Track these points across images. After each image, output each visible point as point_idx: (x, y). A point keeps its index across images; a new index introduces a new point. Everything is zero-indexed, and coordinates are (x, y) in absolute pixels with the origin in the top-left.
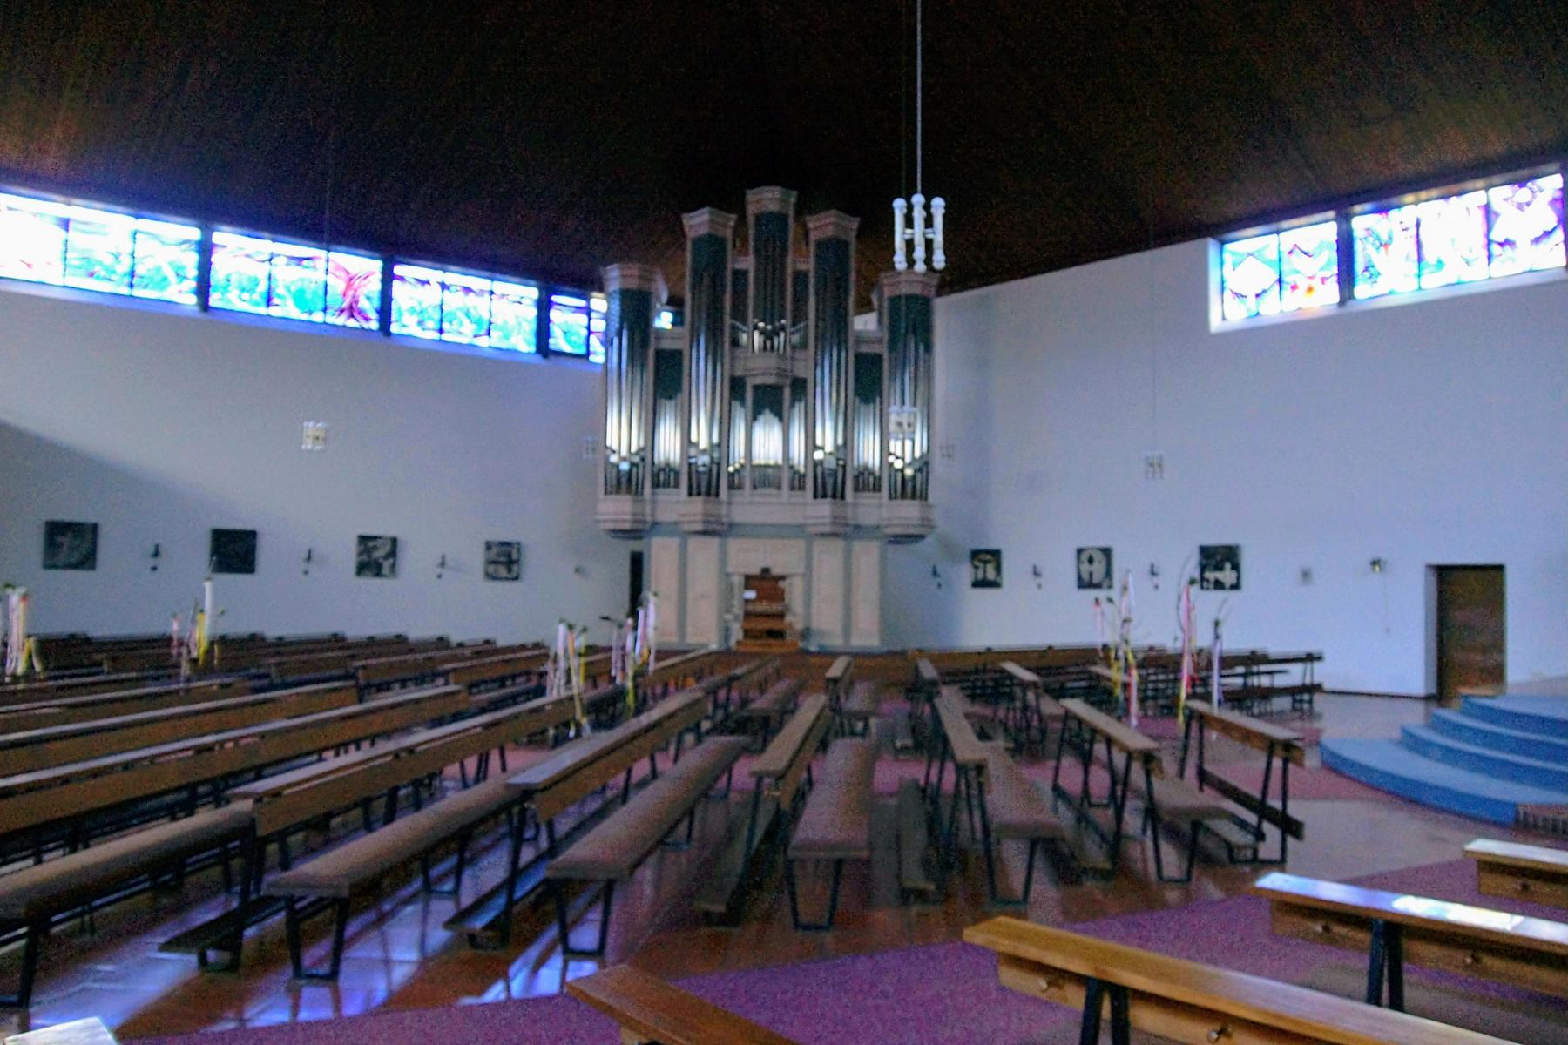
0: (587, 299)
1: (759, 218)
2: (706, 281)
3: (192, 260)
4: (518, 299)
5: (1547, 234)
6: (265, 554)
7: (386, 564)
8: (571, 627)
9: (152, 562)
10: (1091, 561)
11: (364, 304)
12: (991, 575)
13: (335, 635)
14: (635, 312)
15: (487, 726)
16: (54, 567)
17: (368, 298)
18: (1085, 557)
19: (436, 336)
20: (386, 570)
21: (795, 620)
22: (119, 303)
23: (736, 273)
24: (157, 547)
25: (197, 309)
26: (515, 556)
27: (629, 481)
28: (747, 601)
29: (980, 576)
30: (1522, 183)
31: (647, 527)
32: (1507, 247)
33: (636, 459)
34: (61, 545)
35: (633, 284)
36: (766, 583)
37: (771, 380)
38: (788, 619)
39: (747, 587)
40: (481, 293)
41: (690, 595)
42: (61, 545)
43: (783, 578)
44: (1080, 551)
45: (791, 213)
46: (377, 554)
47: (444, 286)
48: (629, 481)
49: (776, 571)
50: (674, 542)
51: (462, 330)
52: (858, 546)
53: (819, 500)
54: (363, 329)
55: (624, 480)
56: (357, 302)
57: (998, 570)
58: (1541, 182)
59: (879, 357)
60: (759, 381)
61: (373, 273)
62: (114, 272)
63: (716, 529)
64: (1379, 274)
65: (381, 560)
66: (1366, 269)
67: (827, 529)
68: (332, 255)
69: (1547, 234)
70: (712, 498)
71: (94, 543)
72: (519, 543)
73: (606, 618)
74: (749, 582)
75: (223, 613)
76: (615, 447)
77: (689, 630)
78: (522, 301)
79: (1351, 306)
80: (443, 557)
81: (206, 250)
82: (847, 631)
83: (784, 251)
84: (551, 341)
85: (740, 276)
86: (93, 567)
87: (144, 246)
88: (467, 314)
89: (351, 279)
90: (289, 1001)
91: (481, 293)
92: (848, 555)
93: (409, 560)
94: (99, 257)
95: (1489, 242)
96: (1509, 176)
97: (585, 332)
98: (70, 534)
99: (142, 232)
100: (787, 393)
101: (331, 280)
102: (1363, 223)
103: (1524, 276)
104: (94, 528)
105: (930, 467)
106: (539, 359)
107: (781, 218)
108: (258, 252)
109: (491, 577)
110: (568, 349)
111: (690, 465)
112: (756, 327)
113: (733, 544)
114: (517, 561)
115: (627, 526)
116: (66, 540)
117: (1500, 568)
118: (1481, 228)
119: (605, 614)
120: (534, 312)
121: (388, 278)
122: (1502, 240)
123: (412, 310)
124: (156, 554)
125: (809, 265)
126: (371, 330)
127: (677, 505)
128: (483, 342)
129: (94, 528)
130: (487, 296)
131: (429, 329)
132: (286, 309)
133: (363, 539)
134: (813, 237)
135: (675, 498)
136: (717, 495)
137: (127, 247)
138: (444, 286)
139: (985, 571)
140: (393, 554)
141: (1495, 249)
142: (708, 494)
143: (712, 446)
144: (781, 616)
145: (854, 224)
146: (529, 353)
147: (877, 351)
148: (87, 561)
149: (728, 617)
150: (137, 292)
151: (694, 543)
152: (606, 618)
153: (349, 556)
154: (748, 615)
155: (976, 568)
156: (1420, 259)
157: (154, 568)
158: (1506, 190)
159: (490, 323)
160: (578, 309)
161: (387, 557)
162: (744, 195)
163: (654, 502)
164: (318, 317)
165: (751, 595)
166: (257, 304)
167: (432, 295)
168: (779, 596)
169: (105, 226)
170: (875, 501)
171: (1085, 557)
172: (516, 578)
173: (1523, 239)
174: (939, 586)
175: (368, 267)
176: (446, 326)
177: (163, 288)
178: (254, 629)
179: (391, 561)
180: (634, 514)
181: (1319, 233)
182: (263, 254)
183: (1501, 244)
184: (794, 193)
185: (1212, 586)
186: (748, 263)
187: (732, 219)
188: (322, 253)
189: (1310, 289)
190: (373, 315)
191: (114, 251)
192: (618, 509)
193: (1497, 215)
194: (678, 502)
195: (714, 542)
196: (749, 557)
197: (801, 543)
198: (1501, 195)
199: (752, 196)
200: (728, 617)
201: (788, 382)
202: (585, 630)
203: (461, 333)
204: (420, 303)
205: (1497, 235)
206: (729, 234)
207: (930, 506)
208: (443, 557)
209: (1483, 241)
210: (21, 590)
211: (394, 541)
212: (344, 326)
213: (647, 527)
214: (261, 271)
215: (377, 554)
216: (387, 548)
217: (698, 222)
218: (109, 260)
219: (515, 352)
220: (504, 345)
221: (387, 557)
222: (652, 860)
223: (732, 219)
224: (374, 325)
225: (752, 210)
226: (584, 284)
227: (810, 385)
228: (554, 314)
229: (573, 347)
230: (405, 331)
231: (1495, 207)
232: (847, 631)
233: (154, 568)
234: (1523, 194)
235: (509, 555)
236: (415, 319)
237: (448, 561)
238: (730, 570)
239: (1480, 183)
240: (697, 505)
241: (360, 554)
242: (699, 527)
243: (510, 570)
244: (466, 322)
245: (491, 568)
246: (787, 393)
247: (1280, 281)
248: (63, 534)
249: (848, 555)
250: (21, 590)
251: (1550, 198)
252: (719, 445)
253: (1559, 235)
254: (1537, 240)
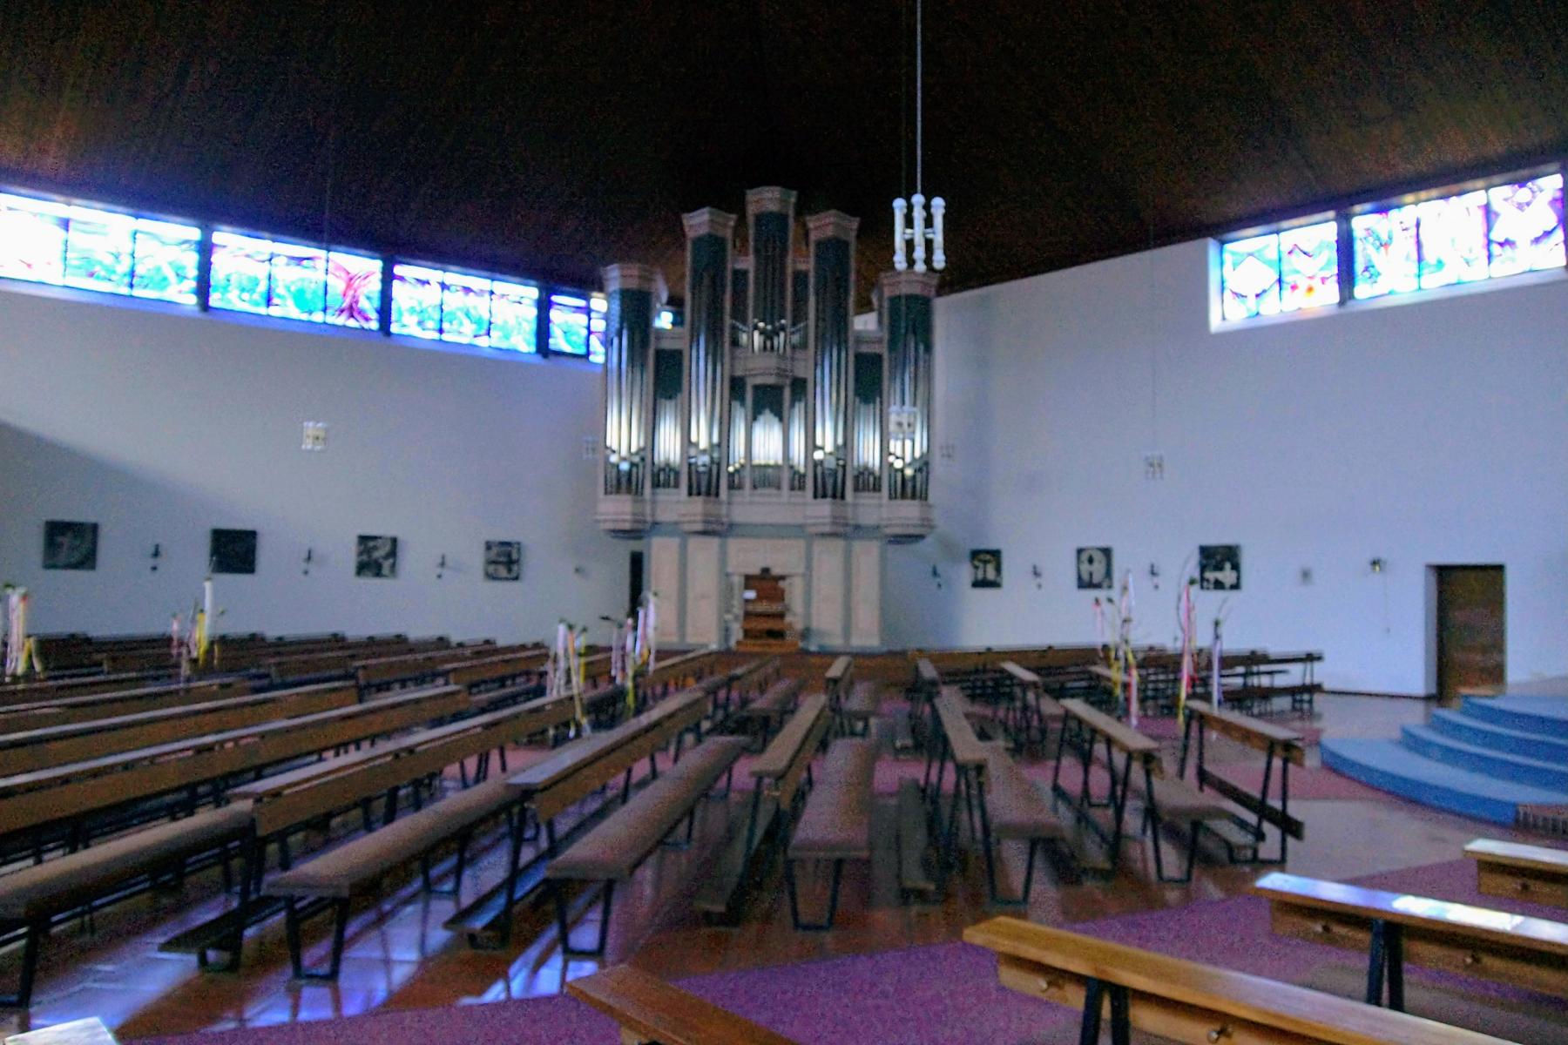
0: (587, 299)
1: (759, 218)
2: (706, 281)
3: (192, 260)
4: (518, 299)
5: (1547, 234)
6: (265, 554)
7: (386, 564)
8: (571, 627)
9: (152, 562)
10: (1091, 561)
11: (364, 304)
12: (991, 575)
13: (335, 635)
14: (635, 312)
16: (54, 567)
17: (368, 298)
18: (1085, 557)
19: (436, 336)
20: (386, 570)
21: (795, 620)
22: (119, 303)
23: (736, 273)
24: (157, 547)
25: (197, 309)
26: (515, 556)
27: (629, 481)
28: (747, 601)
29: (980, 576)
30: (1522, 183)
31: (647, 527)
32: (1507, 247)
33: (636, 459)
34: (61, 545)
35: (633, 284)
36: (766, 583)
37: (771, 380)
38: (788, 619)
39: (747, 587)
40: (481, 293)
41: (690, 595)
42: (61, 545)
43: (783, 578)
44: (1080, 551)
45: (791, 213)
46: (377, 554)
47: (444, 286)
48: (629, 481)
49: (776, 571)
50: (674, 542)
51: (462, 330)
52: (858, 546)
53: (819, 500)
54: (363, 329)
55: (624, 480)
56: (357, 302)
57: (998, 570)
58: (1541, 182)
59: (879, 357)
60: (759, 381)
61: (373, 273)
62: (114, 272)
63: (716, 529)
64: (1379, 274)
65: (381, 560)
66: (1366, 269)
67: (827, 529)
68: (332, 255)
69: (1547, 234)
70: (712, 498)
71: (94, 543)
72: (519, 543)
73: (606, 618)
74: (749, 582)
76: (615, 447)
77: (689, 630)
78: (522, 301)
79: (1351, 306)
80: (443, 557)
81: (206, 250)
82: (847, 631)
83: (784, 251)
84: (551, 341)
85: (740, 276)
86: (93, 567)
87: (144, 246)
88: (467, 314)
89: (351, 279)
91: (481, 293)
92: (848, 555)
93: (409, 560)
94: (99, 257)
95: (1489, 242)
96: (1509, 176)
97: (585, 332)
98: (70, 534)
99: (142, 232)
100: (787, 393)
101: (331, 280)
102: (1363, 223)
103: (1524, 276)
104: (94, 528)
105: (930, 467)
106: (539, 359)
107: (781, 218)
108: (258, 252)
109: (491, 577)
110: (568, 349)
111: (690, 465)
112: (756, 327)
113: (733, 544)
114: (517, 561)
115: (627, 526)
116: (66, 540)
117: (1500, 568)
118: (1481, 228)
119: (605, 614)
120: (534, 312)
121: (388, 278)
122: (1502, 240)
123: (412, 310)
124: (156, 554)
125: (809, 265)
126: (371, 330)
127: (677, 505)
128: (483, 342)
129: (94, 528)
130: (487, 296)
131: (429, 329)
132: (286, 309)
133: (363, 539)
134: (813, 237)
135: (675, 498)
136: (717, 495)
137: (127, 247)
138: (444, 286)
139: (985, 571)
140: (393, 554)
141: (1495, 249)
142: (708, 494)
143: (712, 446)
144: (781, 616)
145: (854, 224)
146: (529, 353)
147: (877, 351)
148: (87, 561)
149: (728, 617)
150: (137, 292)
151: (694, 543)
152: (606, 618)
153: (349, 556)
154: (748, 615)
155: (976, 568)
156: (1420, 259)
157: (154, 568)
158: (1506, 190)
159: (490, 323)
160: (578, 309)
161: (387, 557)
162: (744, 195)
163: (654, 502)
164: (318, 317)
165: (751, 595)
166: (257, 304)
167: (432, 295)
168: (779, 596)
169: (105, 226)
170: (875, 501)
171: (1085, 557)
172: (516, 578)
173: (1523, 239)
174: (939, 586)
175: (368, 267)
176: (446, 326)
177: (163, 288)
178: (254, 629)
179: (391, 561)
180: (634, 514)
181: (1319, 233)
182: (263, 254)
183: (1501, 244)
184: (794, 193)
185: (1212, 586)
186: (748, 263)
187: (732, 219)
188: (322, 253)
189: (1310, 289)
190: (373, 315)
191: (114, 251)
192: (618, 509)
193: (1497, 215)
194: (678, 502)
195: (714, 542)
196: (749, 557)
197: (801, 543)
198: (1501, 195)
199: (752, 196)
200: (728, 617)
201: (788, 382)
202: (585, 630)
203: (461, 333)
204: (420, 303)
205: (1497, 235)
206: (729, 234)
207: (930, 506)
208: (443, 557)
209: (1483, 241)
210: (21, 590)
211: (394, 541)
212: (344, 326)
213: (647, 527)
214: (261, 271)
215: (377, 554)
216: (387, 548)
217: (698, 222)
218: (109, 260)
219: (515, 352)
220: (504, 345)
221: (387, 557)
222: (652, 860)
223: (732, 219)
224: (374, 325)
225: (752, 210)
226: (584, 284)
227: (810, 385)
228: (554, 314)
229: (573, 347)
230: (405, 331)
231: (1495, 207)
232: (847, 631)
233: (154, 568)
234: (1523, 194)
235: (509, 555)
236: (415, 319)
237: (448, 561)
238: (730, 570)
239: (1480, 183)
240: (697, 505)
241: (360, 554)
242: (699, 527)
243: (510, 570)
244: (466, 322)
245: (491, 568)
246: (787, 393)
247: (1280, 281)
248: (63, 534)
249: (848, 555)
250: (21, 590)
251: (1550, 198)
252: (719, 445)
253: (1559, 235)
254: (1537, 240)
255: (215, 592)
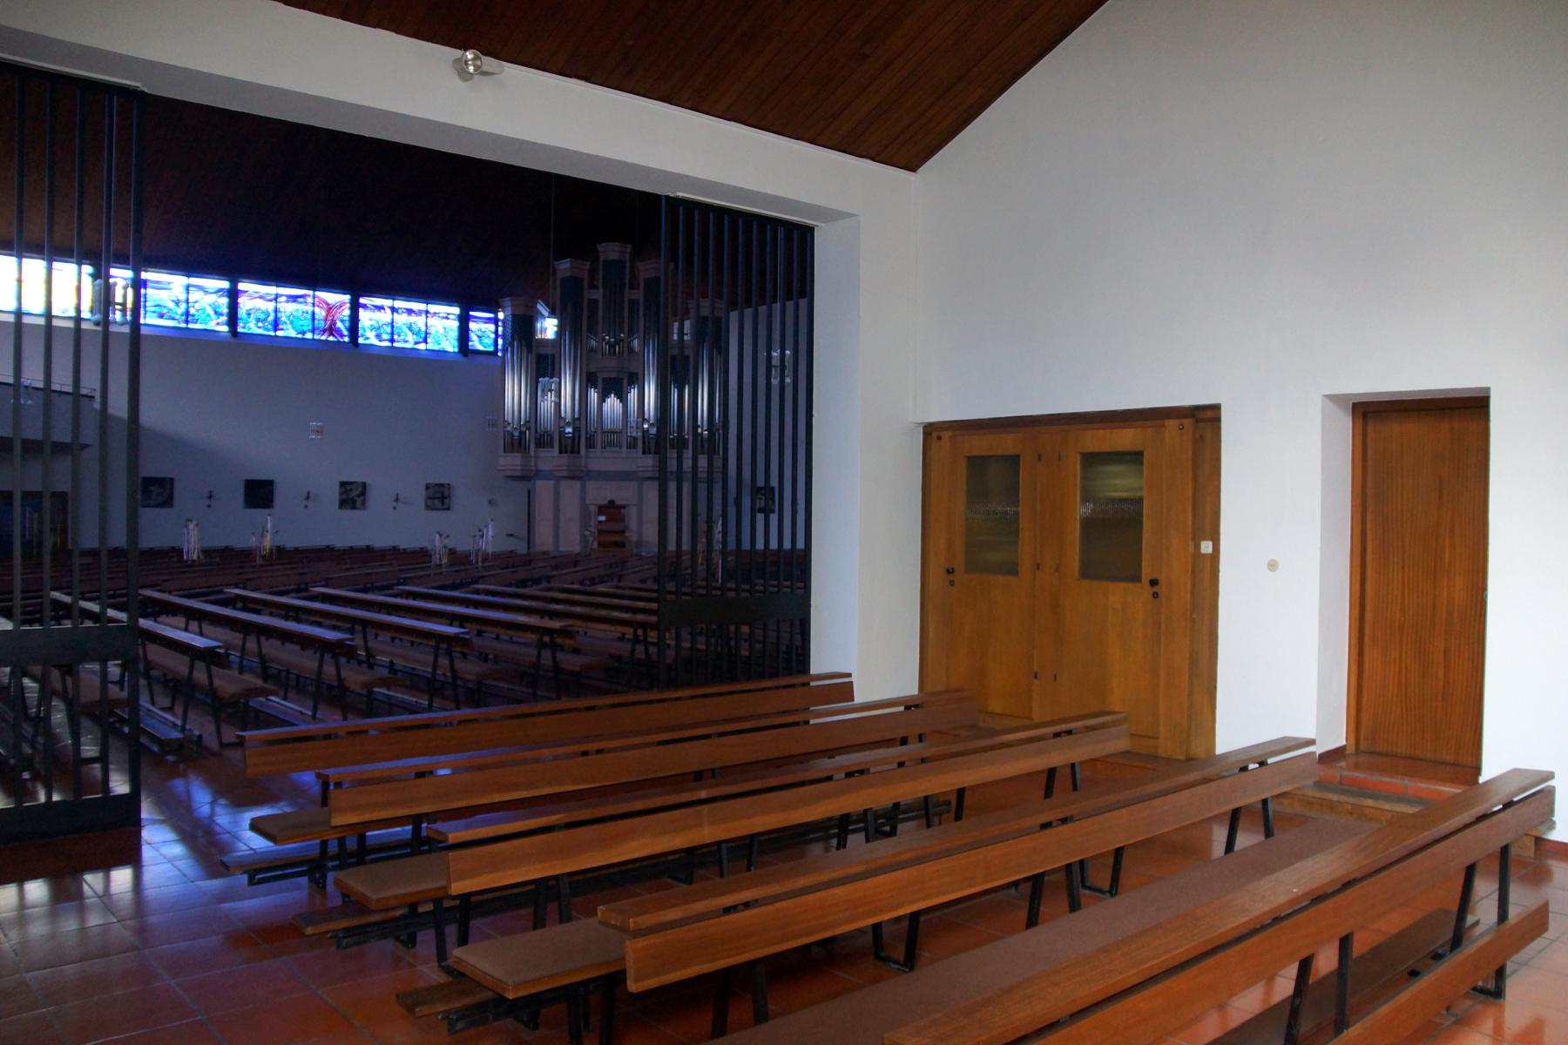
0: (496, 313)
2: (569, 310)
3: (224, 302)
4: (445, 315)
7: (359, 501)
8: (440, 535)
9: (207, 502)
11: (339, 325)
14: (522, 330)
15: (508, 689)
17: (342, 321)
19: (389, 344)
20: (359, 504)
21: (632, 536)
23: (590, 300)
24: (211, 492)
25: (229, 335)
26: (446, 494)
27: (520, 443)
28: (600, 522)
31: (532, 474)
33: (523, 429)
35: (521, 311)
36: (613, 510)
37: (613, 375)
38: (627, 534)
39: (600, 513)
40: (419, 313)
43: (623, 507)
46: (353, 494)
47: (393, 310)
48: (520, 443)
49: (618, 502)
50: (551, 483)
51: (407, 339)
53: (647, 456)
54: (339, 341)
55: (516, 443)
56: (335, 324)
60: (606, 375)
63: (578, 475)
65: (355, 498)
68: (317, 293)
70: (575, 455)
72: (449, 485)
73: (511, 535)
74: (602, 509)
75: (277, 532)
76: (510, 421)
78: (450, 316)
80: (397, 495)
81: (233, 295)
84: (470, 343)
85: (593, 304)
86: (171, 506)
87: (195, 295)
88: (410, 328)
89: (331, 308)
90: (323, 676)
91: (419, 313)
93: (374, 497)
97: (493, 336)
100: (625, 382)
101: (317, 310)
106: (460, 358)
107: (620, 264)
108: (268, 294)
109: (428, 507)
110: (481, 348)
111: (560, 432)
112: (604, 340)
113: (590, 485)
114: (449, 497)
115: (518, 474)
119: (509, 532)
120: (456, 324)
121: (355, 307)
123: (373, 328)
124: (210, 497)
125: (639, 295)
126: (345, 342)
127: (550, 459)
128: (422, 346)
130: (424, 315)
131: (385, 340)
132: (288, 331)
133: (343, 484)
136: (579, 452)
137: (183, 297)
138: (393, 310)
140: (363, 493)
142: (572, 452)
143: (574, 419)
144: (622, 532)
146: (454, 352)
148: (168, 502)
149: (587, 533)
151: (563, 484)
152: (511, 535)
153: (334, 495)
154: (600, 532)
157: (209, 506)
159: (426, 333)
160: (488, 320)
161: (359, 496)
163: (536, 457)
164: (309, 336)
165: (602, 518)
166: (269, 330)
167: (385, 317)
168: (622, 519)
169: (169, 283)
172: (448, 509)
175: (338, 298)
176: (396, 337)
177: (206, 324)
179: (362, 498)
180: (521, 465)
182: (271, 295)
184: (629, 246)
186: (598, 295)
188: (311, 292)
190: (345, 332)
191: (175, 299)
192: (514, 461)
195: (577, 484)
196: (600, 493)
200: (587, 533)
201: (626, 375)
202: (448, 536)
203: (407, 341)
204: (378, 322)
206: (586, 276)
208: (397, 495)
210: (194, 522)
211: (364, 485)
213: (532, 474)
214: (271, 306)
215: (353, 494)
216: (360, 490)
217: (565, 266)
218: (172, 305)
219: (445, 352)
220: (436, 348)
221: (359, 496)
224: (346, 339)
226: (492, 306)
227: (640, 376)
229: (485, 347)
230: (367, 342)
233: (209, 506)
235: (442, 493)
236: (374, 333)
237: (401, 497)
238: (588, 502)
240: (564, 460)
241: (341, 494)
242: (565, 474)
243: (443, 503)
244: (410, 334)
245: (430, 502)
246: (625, 382)
250: (194, 522)
252: (579, 419)
255: (123, 334)
